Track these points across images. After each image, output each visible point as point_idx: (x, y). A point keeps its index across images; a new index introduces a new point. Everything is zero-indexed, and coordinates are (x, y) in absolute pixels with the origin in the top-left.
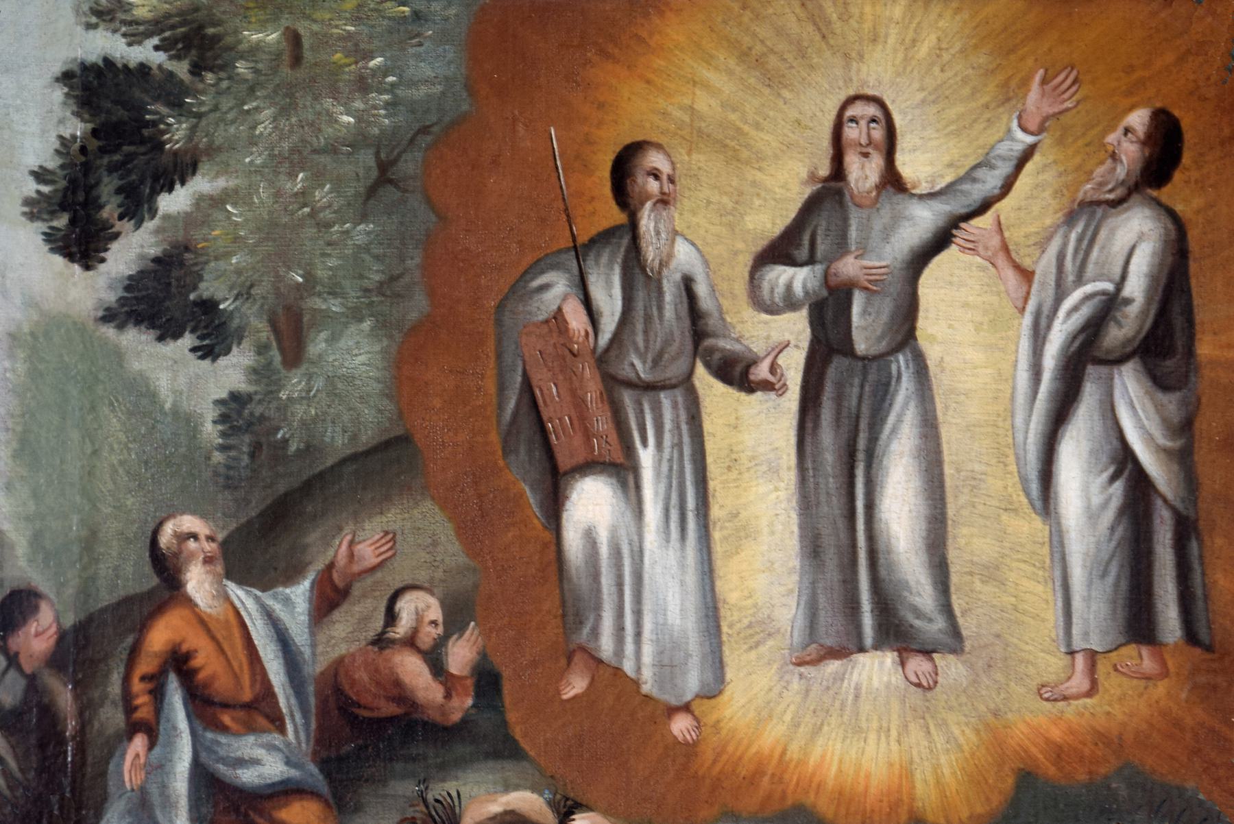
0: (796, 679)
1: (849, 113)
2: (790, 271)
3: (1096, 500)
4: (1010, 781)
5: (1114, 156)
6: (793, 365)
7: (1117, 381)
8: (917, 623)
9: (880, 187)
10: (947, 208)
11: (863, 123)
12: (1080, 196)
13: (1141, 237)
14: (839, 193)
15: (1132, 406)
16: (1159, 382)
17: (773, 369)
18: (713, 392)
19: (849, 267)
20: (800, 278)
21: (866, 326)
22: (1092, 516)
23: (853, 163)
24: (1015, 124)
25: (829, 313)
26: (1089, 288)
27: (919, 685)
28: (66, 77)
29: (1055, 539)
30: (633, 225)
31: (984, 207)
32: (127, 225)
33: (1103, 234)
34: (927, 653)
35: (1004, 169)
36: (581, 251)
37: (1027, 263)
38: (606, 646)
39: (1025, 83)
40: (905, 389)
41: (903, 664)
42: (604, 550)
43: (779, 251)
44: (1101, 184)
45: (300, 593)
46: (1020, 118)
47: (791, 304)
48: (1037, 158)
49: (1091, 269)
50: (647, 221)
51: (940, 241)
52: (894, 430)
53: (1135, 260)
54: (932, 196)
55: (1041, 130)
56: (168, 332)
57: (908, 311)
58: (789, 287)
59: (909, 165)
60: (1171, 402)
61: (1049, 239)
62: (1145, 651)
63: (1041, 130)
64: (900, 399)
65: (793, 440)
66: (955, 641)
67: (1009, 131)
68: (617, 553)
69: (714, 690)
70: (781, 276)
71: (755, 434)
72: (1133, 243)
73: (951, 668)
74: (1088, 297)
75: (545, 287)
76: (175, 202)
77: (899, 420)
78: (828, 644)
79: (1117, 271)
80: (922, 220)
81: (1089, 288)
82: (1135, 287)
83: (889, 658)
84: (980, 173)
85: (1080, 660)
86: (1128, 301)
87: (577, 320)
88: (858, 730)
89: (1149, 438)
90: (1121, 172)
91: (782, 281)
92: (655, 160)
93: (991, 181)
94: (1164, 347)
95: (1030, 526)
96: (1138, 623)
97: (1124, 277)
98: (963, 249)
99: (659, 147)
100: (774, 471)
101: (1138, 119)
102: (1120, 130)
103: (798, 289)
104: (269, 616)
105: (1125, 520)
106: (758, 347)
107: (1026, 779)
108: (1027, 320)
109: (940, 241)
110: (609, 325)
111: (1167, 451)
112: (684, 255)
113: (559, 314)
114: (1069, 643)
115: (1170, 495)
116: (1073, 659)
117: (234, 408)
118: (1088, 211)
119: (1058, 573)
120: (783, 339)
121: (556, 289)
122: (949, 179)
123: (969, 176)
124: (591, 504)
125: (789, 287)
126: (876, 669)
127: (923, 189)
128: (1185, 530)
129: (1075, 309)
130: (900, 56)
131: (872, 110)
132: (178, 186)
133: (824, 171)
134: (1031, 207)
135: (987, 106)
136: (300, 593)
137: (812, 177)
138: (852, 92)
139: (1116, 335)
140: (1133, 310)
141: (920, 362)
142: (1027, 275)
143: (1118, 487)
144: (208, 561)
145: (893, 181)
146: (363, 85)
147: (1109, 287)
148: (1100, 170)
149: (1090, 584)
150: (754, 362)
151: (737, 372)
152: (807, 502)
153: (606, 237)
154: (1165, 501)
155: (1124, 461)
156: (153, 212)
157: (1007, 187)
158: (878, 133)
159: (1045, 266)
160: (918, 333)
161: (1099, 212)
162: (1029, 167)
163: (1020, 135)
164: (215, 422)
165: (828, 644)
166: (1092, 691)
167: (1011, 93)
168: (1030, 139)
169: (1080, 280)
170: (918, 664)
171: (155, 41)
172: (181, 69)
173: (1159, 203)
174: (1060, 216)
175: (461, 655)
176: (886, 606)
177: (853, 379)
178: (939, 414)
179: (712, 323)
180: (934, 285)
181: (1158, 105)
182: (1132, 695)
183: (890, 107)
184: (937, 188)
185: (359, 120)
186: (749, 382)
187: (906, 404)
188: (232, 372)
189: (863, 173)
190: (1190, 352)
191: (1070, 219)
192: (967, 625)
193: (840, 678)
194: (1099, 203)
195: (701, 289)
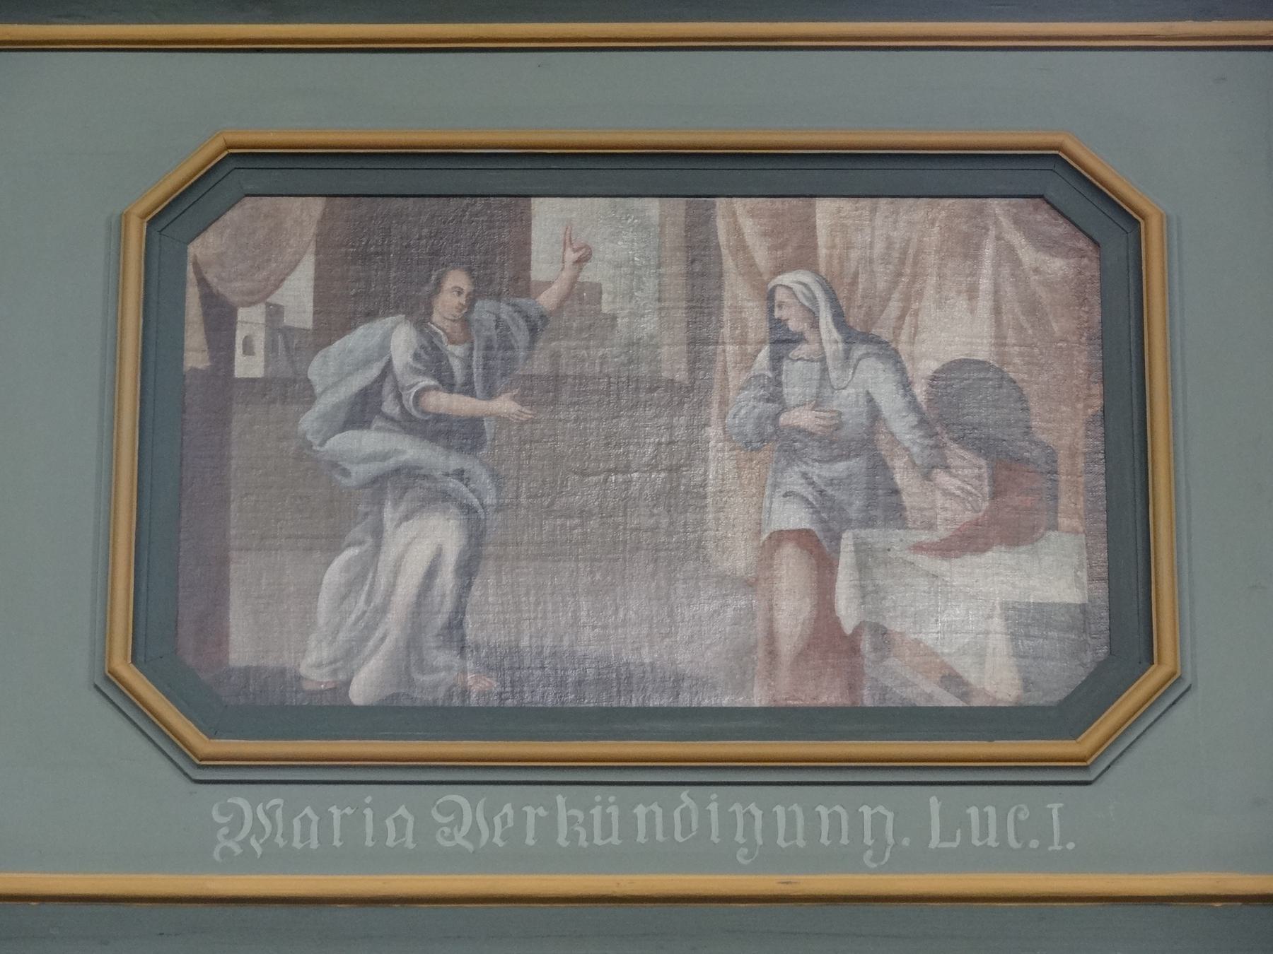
170: (874, 619)
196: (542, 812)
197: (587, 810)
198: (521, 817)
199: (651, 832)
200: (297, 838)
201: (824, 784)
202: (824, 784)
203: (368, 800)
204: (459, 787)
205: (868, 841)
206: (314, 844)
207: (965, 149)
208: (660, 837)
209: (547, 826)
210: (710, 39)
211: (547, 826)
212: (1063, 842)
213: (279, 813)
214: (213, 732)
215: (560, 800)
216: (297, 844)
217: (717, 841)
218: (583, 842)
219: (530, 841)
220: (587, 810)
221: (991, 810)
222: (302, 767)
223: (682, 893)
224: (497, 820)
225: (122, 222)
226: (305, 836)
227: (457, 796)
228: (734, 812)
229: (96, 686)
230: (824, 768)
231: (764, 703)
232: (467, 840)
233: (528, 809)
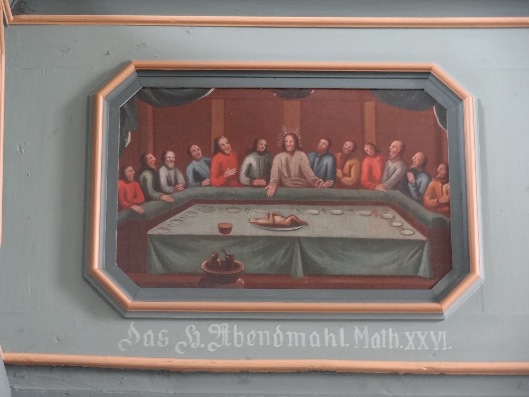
18: (374, 143)
208: (391, 347)
212: (447, 346)
213: (444, 335)
219: (434, 107)
225: (125, 65)
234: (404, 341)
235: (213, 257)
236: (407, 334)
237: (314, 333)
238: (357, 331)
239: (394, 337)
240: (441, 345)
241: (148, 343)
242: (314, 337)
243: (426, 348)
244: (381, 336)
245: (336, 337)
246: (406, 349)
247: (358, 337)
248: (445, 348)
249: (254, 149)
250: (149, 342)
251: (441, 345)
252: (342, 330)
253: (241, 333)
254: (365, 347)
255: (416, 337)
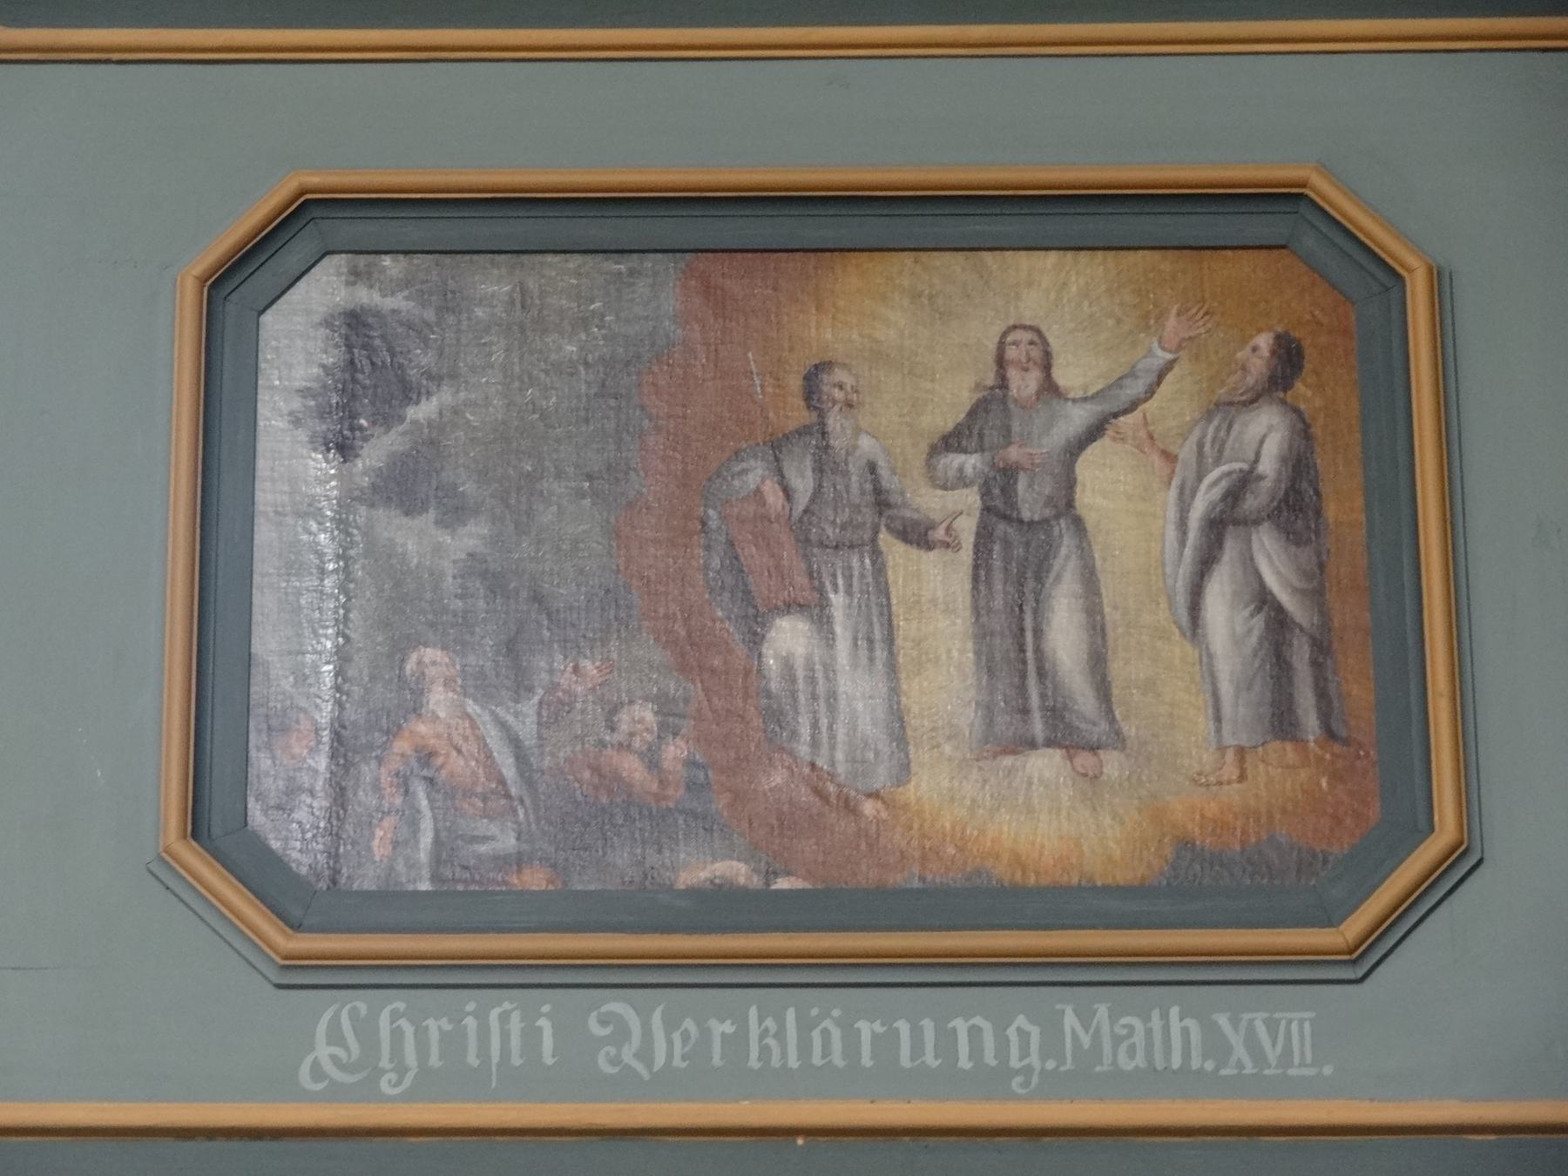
0: (975, 770)
1: (1009, 339)
2: (963, 457)
3: (1239, 629)
4: (1168, 851)
5: (1244, 368)
6: (967, 528)
7: (1254, 537)
8: (1083, 726)
9: (1038, 393)
10: (1099, 408)
11: (1022, 346)
12: (1215, 399)
13: (1270, 428)
14: (1004, 401)
15: (1269, 556)
16: (1293, 537)
17: (948, 529)
18: (896, 552)
19: (1013, 453)
20: (971, 462)
21: (1030, 500)
22: (1237, 642)
23: (1013, 374)
24: (1156, 345)
25: (998, 507)
26: (1225, 468)
27: (1085, 775)
28: (327, 323)
29: (1205, 660)
30: (822, 424)
31: (1132, 407)
32: (378, 430)
33: (1236, 427)
34: (1094, 749)
35: (1152, 378)
36: (777, 446)
37: (1173, 449)
38: (803, 750)
39: (1161, 317)
40: (1067, 545)
41: (1071, 758)
42: (800, 673)
43: (951, 442)
44: (1235, 389)
45: (529, 707)
46: (1160, 342)
47: (962, 481)
48: (1176, 370)
49: (1227, 453)
50: (834, 422)
51: (1094, 432)
52: (1058, 578)
53: (1265, 446)
54: (1085, 399)
55: (1177, 351)
56: (411, 508)
57: (1069, 483)
58: (961, 469)
59: (1064, 376)
60: (1306, 555)
61: (1190, 431)
62: (1289, 746)
63: (1179, 347)
64: (1063, 551)
65: (968, 586)
66: (1118, 740)
67: (1150, 350)
68: (810, 669)
69: (904, 771)
70: (954, 461)
71: (935, 591)
72: (1265, 435)
73: (1113, 764)
74: (1229, 474)
75: (745, 472)
76: (422, 411)
77: (1063, 567)
78: (1005, 739)
79: (1252, 456)
80: (1077, 418)
81: (1225, 468)
82: (1268, 466)
83: (1057, 755)
84: (1127, 382)
85: (1230, 756)
86: (1261, 478)
87: (774, 497)
88: (1030, 811)
89: (1286, 583)
90: (1250, 380)
91: (956, 464)
92: (840, 375)
93: (1136, 388)
94: (1297, 508)
95: (1180, 650)
96: (1282, 722)
97: (1256, 461)
98: (1114, 439)
99: (844, 366)
100: (948, 611)
101: (1264, 341)
102: (1248, 349)
103: (969, 471)
104: (503, 726)
105: (1266, 644)
106: (936, 516)
107: (1185, 844)
108: (1173, 493)
109: (1094, 432)
110: (802, 500)
111: (1303, 592)
112: (865, 443)
113: (758, 491)
114: (1219, 740)
115: (1305, 623)
116: (1223, 756)
117: (474, 567)
118: (1227, 408)
119: (1208, 687)
120: (960, 509)
121: (756, 474)
122: (1100, 387)
123: (1119, 383)
124: (789, 637)
125: (961, 469)
126: (1045, 765)
127: (1080, 394)
128: (1321, 648)
129: (1215, 483)
130: (1053, 295)
131: (1027, 336)
132: (424, 399)
133: (990, 379)
134: (1175, 405)
135: (1131, 332)
136: (529, 707)
137: (978, 386)
138: (1011, 322)
139: (1252, 503)
140: (1267, 484)
141: (1078, 524)
142: (1170, 457)
143: (1259, 622)
144: (448, 683)
145: (1050, 388)
146: (584, 322)
147: (1245, 466)
148: (1232, 379)
149: (1237, 697)
150: (932, 526)
151: (918, 535)
152: (982, 635)
153: (803, 431)
154: (1302, 630)
155: (1264, 600)
156: (402, 419)
157: (1150, 392)
158: (1036, 353)
159: (1186, 452)
160: (1077, 504)
161: (1233, 409)
162: (1169, 377)
163: (1160, 353)
164: (454, 577)
165: (1005, 739)
166: (1242, 777)
167: (1149, 320)
168: (1169, 356)
169: (1218, 462)
170: (1084, 760)
171: (406, 293)
172: (430, 315)
173: (1283, 402)
174: (1197, 415)
175: (674, 752)
176: (1057, 713)
177: (1021, 541)
178: (1098, 563)
179: (895, 499)
180: (1089, 467)
181: (1279, 329)
182: (1278, 777)
183: (1047, 334)
184: (1090, 394)
185: (581, 348)
186: (927, 542)
187: (1068, 557)
188: (471, 537)
189: (1024, 384)
190: (1318, 513)
191: (1209, 415)
192: (1129, 730)
193: (1010, 771)
194: (1231, 404)
195: (884, 472)
196: (879, 1028)
197: (1146, 1018)
198: (705, 1034)
199: (976, 1051)
200: (1014, 1051)
201: (911, 985)
202: (302, 987)
203: (471, 1007)
204: (362, 992)
205: (385, 1063)
206: (839, 1061)
207: (558, 191)
208: (990, 1059)
209: (886, 1044)
210: (212, 50)
211: (886, 1044)
213: (1307, 1025)
214: (1330, 920)
215: (1102, 1011)
216: (839, 1061)
217: (549, 1061)
218: (775, 1062)
219: (717, 1060)
220: (1146, 1018)
221: (928, 1025)
222: (461, 967)
223: (518, 1125)
224: (677, 1037)
226: (826, 1052)
227: (617, 1005)
228: (954, 1030)
229: (151, 872)
230: (1099, 964)
231: (374, 888)
232: (651, 1055)
233: (431, 1023)
234: (1217, 1046)
235: (608, 779)
236: (1223, 1020)
237: (1021, 1021)
238: (1070, 1020)
239: (1185, 1032)
240: (1286, 1057)
241: (824, 1056)
242: (1023, 1035)
243: (1249, 1069)
244: (1149, 1033)
245: (811, 1055)
246: (1224, 1072)
247: (1075, 1037)
248: (1069, 1065)
249: (667, 729)
250: (826, 1052)
251: (1286, 1057)
252: (791, 1015)
253: (770, 1023)
254: (1098, 1069)
255: (1211, 1030)
